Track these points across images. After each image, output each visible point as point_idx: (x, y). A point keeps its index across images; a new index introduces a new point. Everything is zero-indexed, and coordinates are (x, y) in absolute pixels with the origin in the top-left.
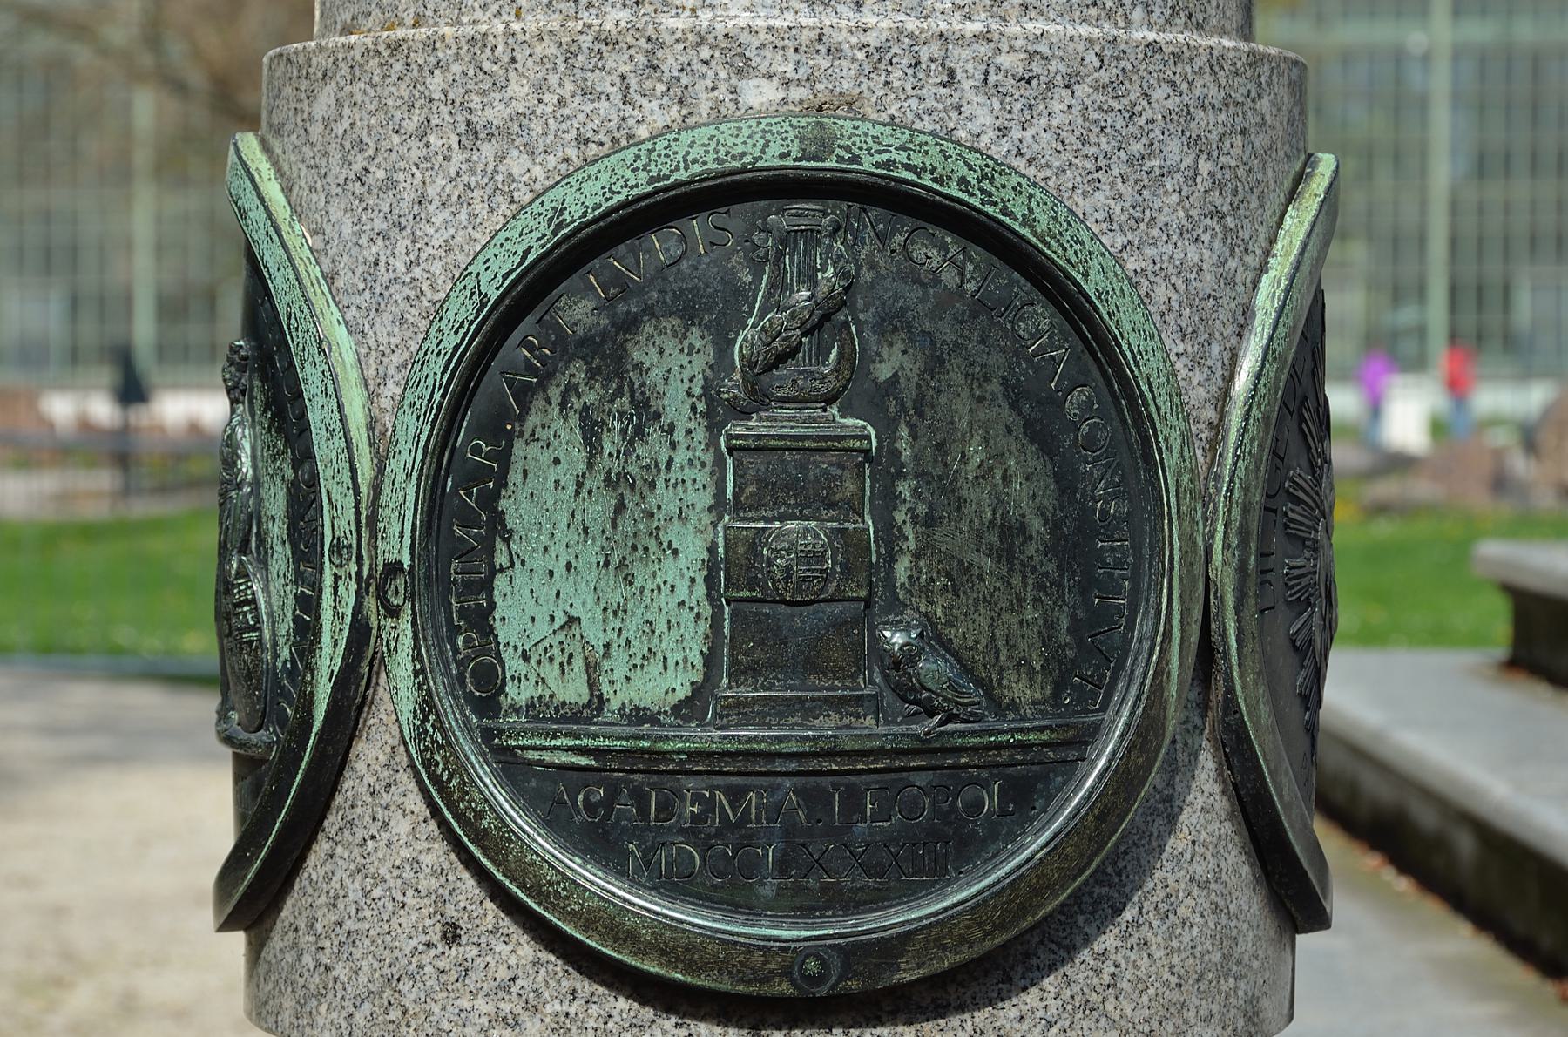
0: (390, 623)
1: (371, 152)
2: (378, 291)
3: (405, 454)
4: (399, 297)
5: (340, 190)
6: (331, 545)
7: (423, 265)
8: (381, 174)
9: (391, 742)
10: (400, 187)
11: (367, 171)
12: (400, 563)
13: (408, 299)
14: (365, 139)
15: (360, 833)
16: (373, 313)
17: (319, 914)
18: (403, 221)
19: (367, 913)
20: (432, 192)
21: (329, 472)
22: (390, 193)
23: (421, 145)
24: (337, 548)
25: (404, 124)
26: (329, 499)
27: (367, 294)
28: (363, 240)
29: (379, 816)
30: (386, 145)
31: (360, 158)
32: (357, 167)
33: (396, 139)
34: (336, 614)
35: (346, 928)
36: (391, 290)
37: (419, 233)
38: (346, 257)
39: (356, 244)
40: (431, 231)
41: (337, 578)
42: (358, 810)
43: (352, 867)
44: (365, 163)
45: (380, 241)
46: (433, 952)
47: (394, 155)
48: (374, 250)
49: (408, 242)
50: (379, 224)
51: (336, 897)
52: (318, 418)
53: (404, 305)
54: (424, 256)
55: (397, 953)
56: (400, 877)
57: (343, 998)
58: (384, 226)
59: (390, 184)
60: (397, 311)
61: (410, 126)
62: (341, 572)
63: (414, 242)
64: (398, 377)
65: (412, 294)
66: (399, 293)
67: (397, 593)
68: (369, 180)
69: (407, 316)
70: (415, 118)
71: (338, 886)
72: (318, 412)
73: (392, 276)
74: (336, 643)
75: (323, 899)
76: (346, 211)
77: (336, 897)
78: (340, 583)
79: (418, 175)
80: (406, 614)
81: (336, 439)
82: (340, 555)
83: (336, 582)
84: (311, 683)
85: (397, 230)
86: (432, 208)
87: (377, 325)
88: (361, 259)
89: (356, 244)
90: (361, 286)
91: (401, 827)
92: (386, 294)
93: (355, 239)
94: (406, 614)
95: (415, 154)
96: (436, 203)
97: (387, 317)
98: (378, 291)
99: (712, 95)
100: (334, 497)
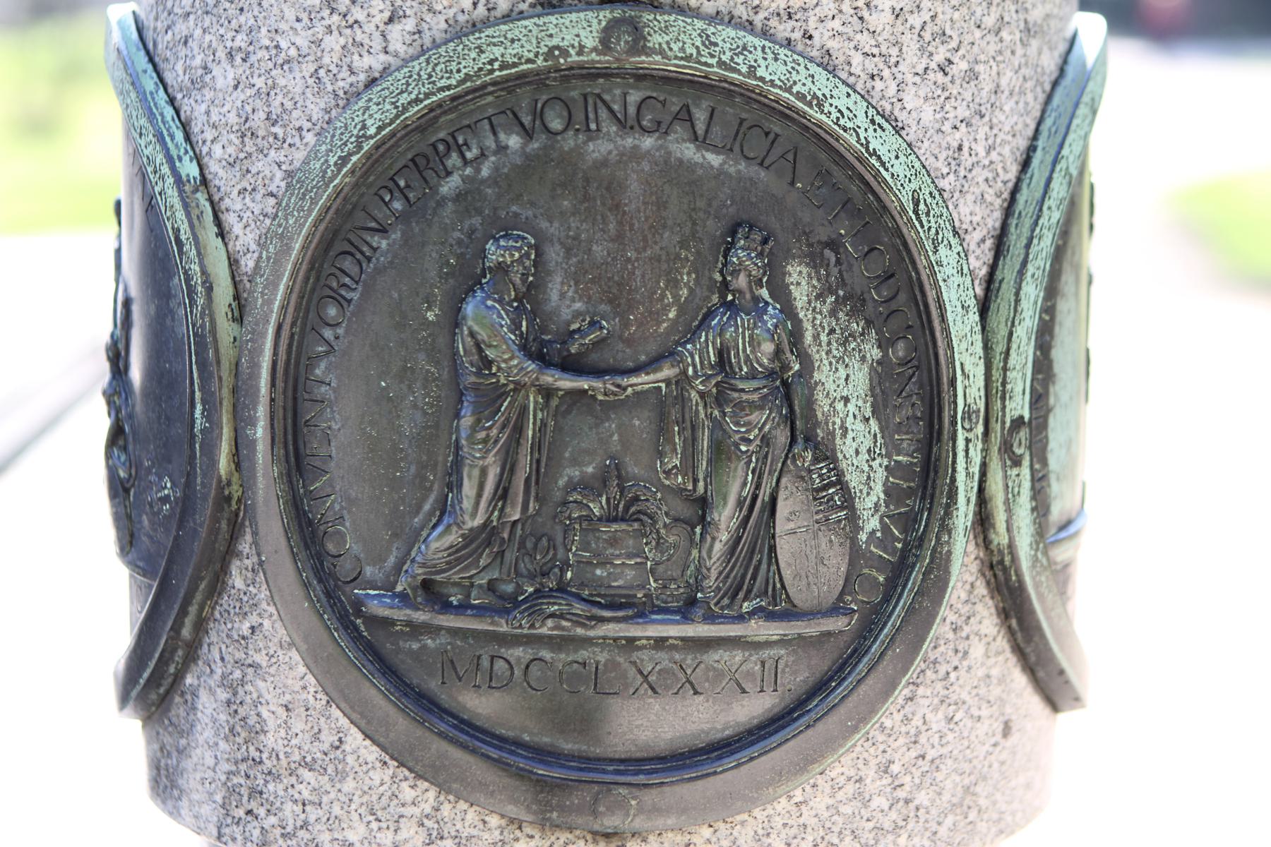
0: (1015, 471)
1: (954, 44)
2: (962, 174)
3: (1027, 319)
4: (981, 179)
5: (917, 79)
6: (964, 412)
7: (998, 149)
8: (964, 66)
9: (971, 579)
10: (981, 78)
11: (950, 62)
12: (1022, 417)
13: (987, 180)
14: (948, 32)
15: (943, 669)
16: (957, 195)
17: (897, 756)
18: (983, 108)
19: (950, 737)
20: (1004, 82)
21: (964, 345)
22: (972, 83)
23: (997, 39)
24: (968, 414)
25: (984, 19)
26: (963, 370)
27: (952, 177)
28: (947, 127)
29: (960, 648)
30: (968, 38)
31: (942, 49)
32: (939, 58)
33: (978, 33)
34: (968, 474)
35: (928, 758)
36: (974, 172)
37: (995, 121)
38: (926, 143)
39: (939, 131)
40: (1002, 118)
41: (968, 441)
42: (942, 649)
43: (936, 701)
44: (948, 55)
45: (963, 127)
46: (999, 748)
47: (976, 48)
48: (958, 135)
49: (987, 128)
50: (963, 112)
51: (918, 733)
52: (954, 296)
53: (984, 186)
54: (998, 140)
55: (975, 762)
56: (977, 695)
57: (926, 821)
58: (967, 114)
59: (972, 75)
60: (978, 191)
61: (990, 21)
62: (971, 435)
63: (991, 128)
64: (978, 252)
65: (990, 176)
66: (980, 175)
67: (1020, 444)
68: (953, 70)
69: (986, 196)
70: (992, 15)
71: (920, 723)
72: (953, 292)
73: (974, 159)
74: (968, 501)
75: (901, 741)
76: (926, 99)
77: (918, 733)
78: (971, 445)
79: (995, 68)
80: (1026, 462)
81: (971, 314)
82: (970, 420)
83: (967, 446)
84: (948, 543)
85: (978, 117)
86: (1004, 97)
87: (961, 206)
88: (944, 145)
89: (939, 131)
90: (945, 170)
91: (977, 650)
92: (969, 176)
93: (937, 126)
94: (1026, 462)
95: (992, 49)
96: (1007, 93)
97: (970, 198)
98: (962, 174)
99: (310, 32)
100: (967, 368)
